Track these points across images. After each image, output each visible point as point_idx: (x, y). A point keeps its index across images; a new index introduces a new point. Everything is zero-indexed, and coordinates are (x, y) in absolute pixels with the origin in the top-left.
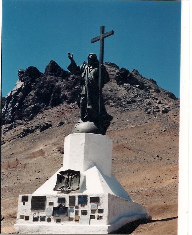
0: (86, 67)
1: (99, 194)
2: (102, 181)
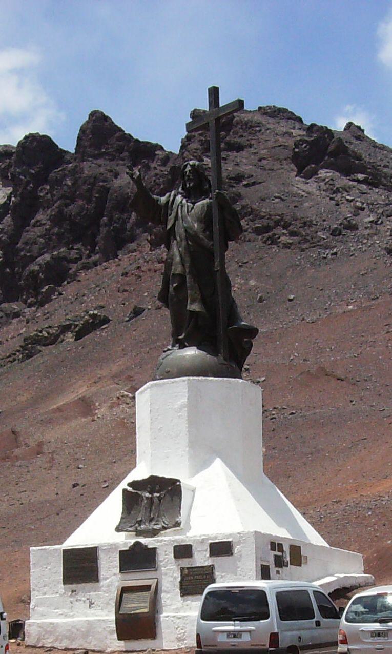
0: (179, 198)
1: (230, 535)
2: (239, 500)
